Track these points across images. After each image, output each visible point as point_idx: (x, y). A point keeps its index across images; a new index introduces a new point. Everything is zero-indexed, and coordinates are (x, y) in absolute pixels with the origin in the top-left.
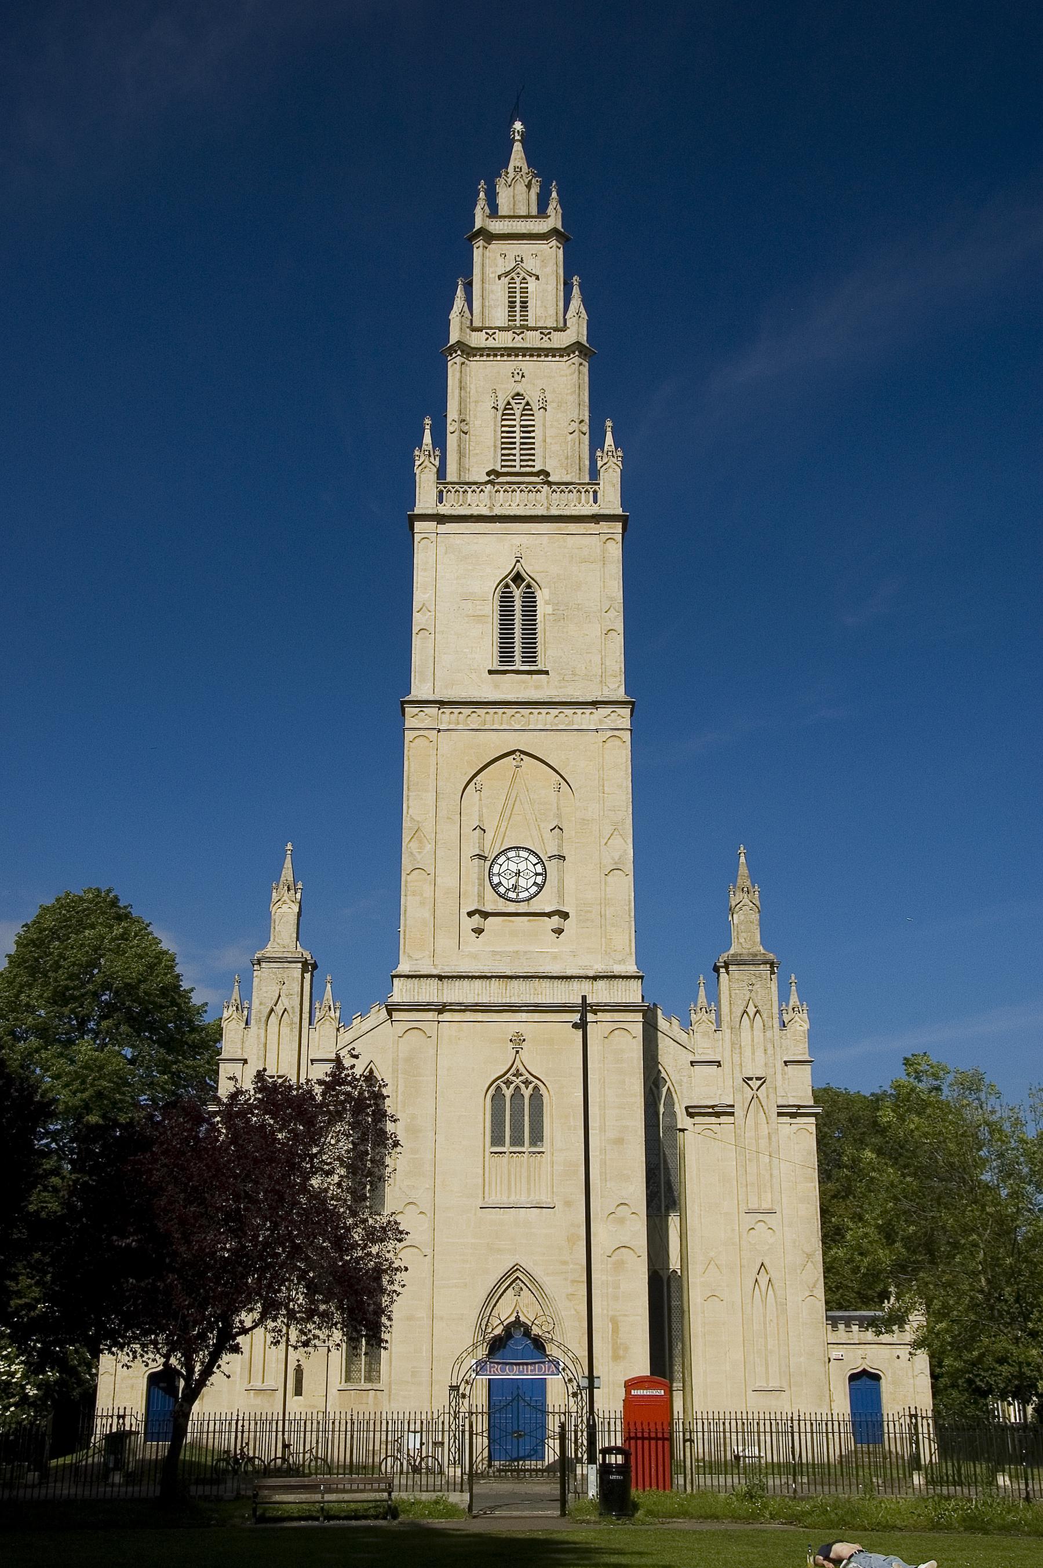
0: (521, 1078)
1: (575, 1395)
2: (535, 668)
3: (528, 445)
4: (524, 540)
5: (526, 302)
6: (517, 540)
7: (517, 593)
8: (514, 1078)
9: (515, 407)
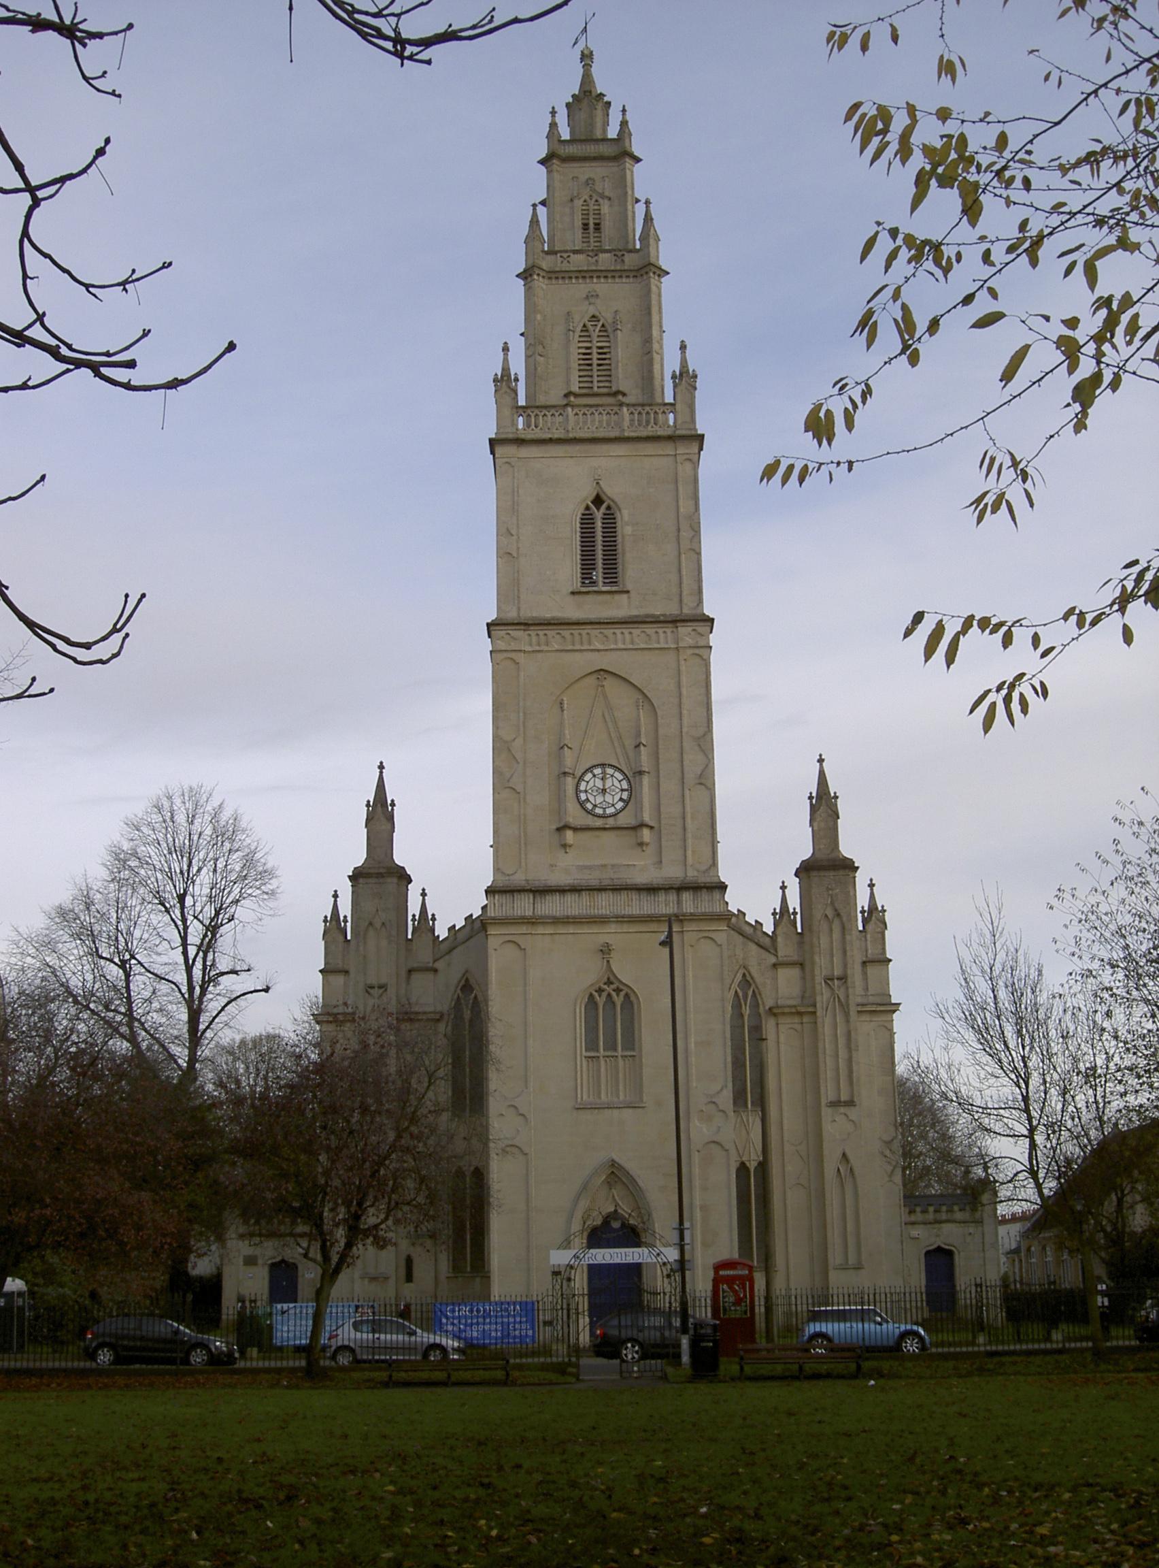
0: (612, 987)
1: (669, 1276)
2: (614, 589)
7: (599, 515)
9: (591, 329)
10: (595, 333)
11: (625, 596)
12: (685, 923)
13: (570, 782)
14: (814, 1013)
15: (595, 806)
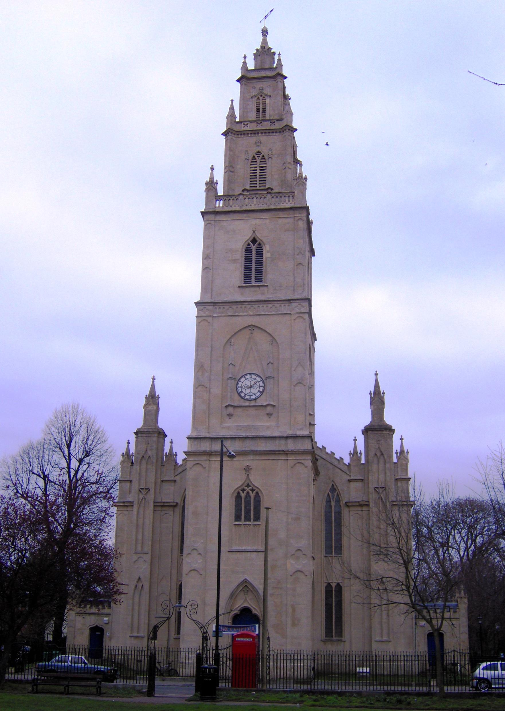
3: (263, 177)
4: (257, 222)
5: (265, 109)
6: (253, 222)
7: (254, 248)
8: (246, 488)
9: (257, 158)
10: (258, 160)
11: (265, 288)
12: (289, 455)
13: (232, 383)
14: (368, 505)
15: (246, 395)
